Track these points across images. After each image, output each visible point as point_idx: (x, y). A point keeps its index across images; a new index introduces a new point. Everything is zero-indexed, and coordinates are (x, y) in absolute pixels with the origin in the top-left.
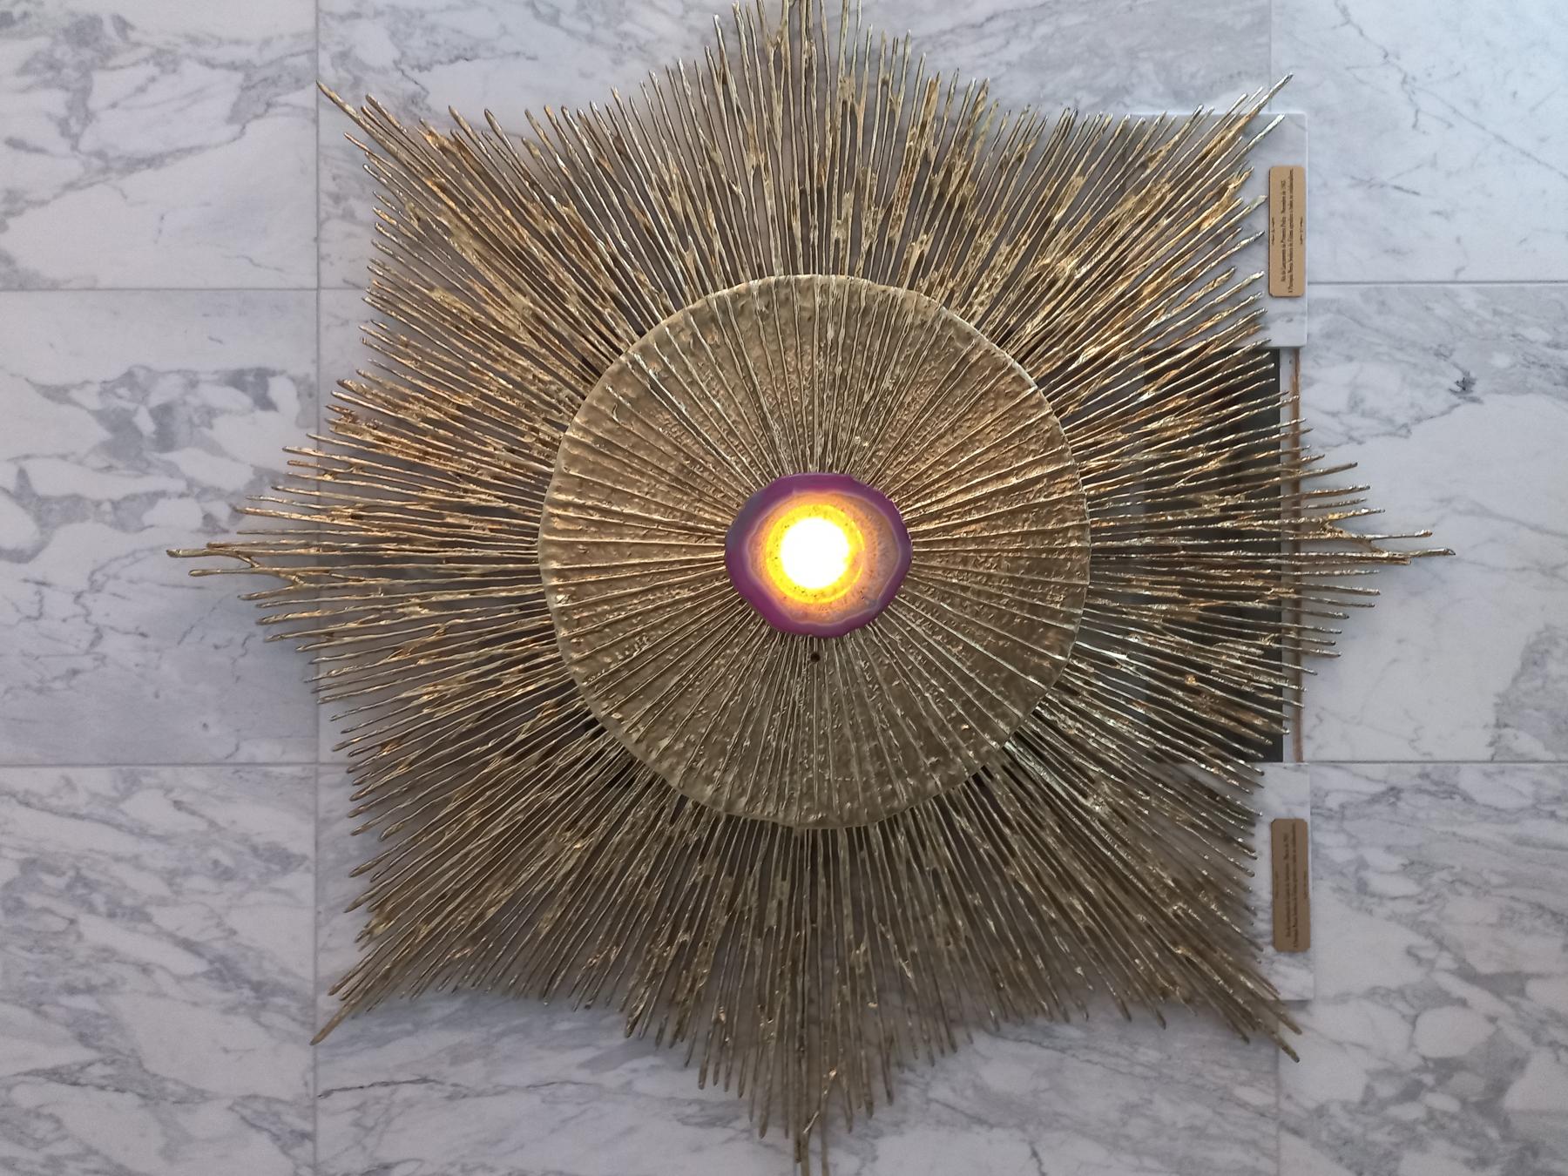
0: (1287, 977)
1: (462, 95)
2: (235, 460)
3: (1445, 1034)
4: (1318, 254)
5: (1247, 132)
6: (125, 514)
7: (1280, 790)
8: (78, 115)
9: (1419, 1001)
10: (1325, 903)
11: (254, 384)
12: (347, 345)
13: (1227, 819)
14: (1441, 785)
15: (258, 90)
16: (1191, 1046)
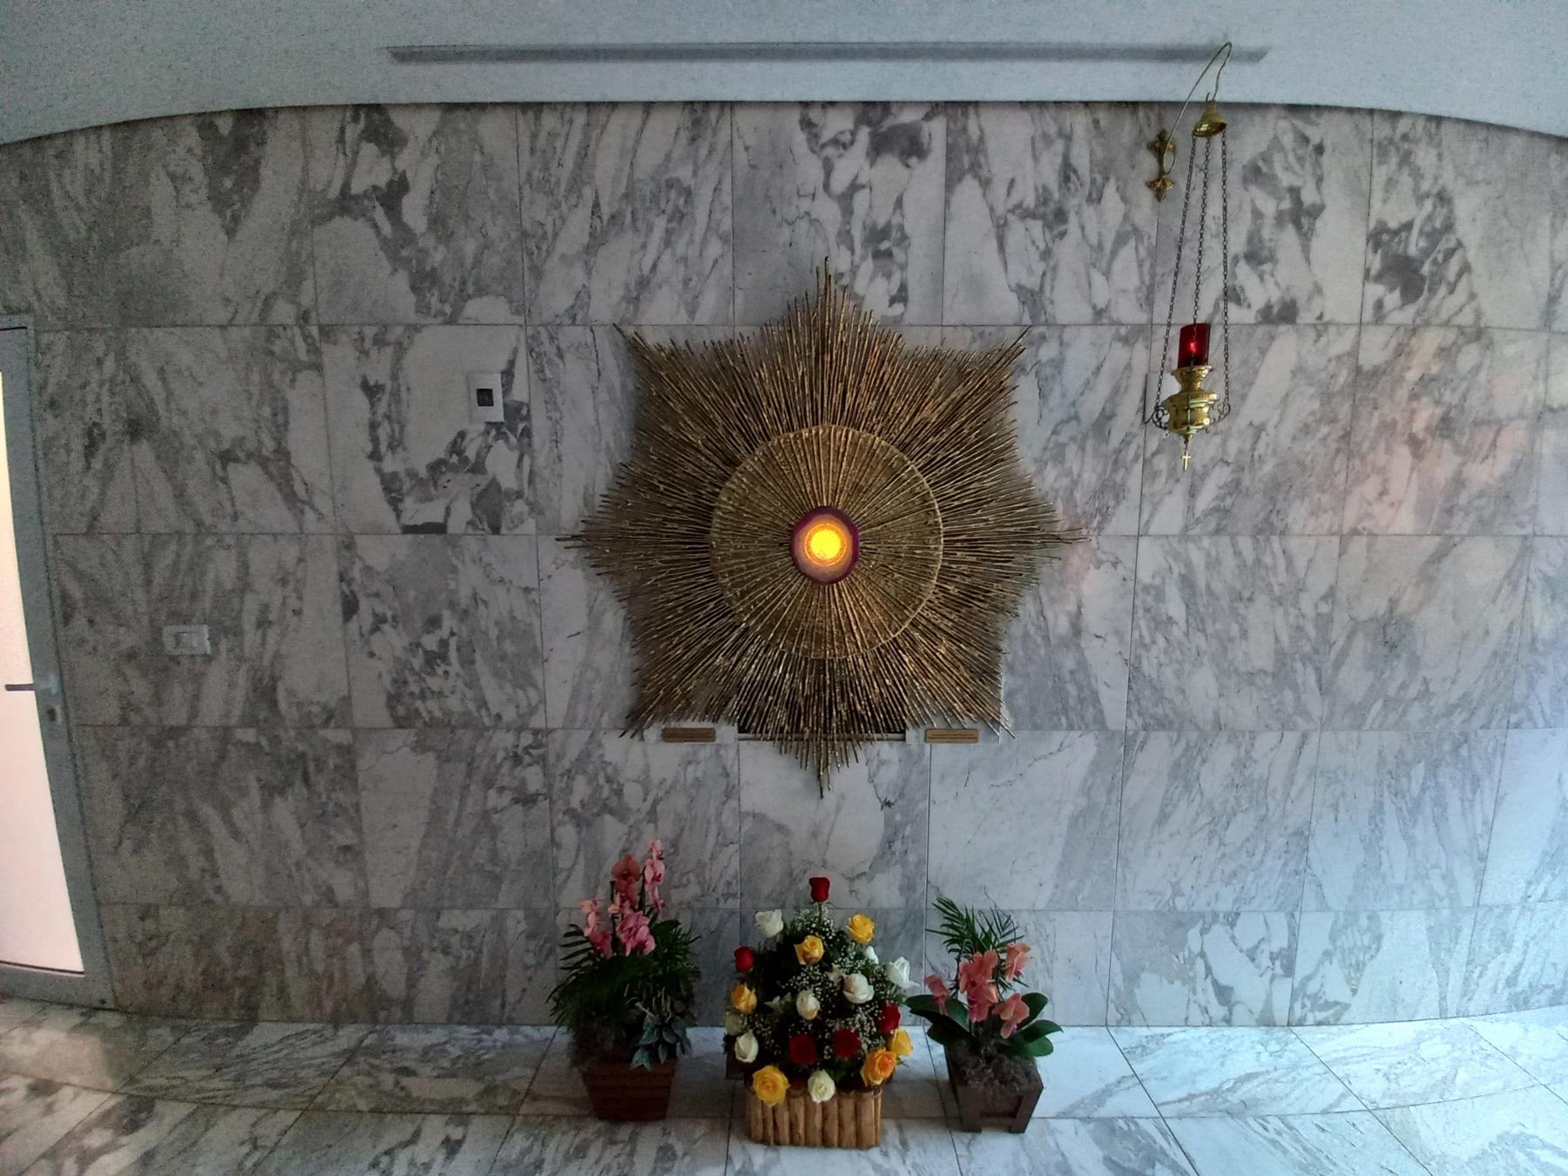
0: (652, 733)
3: (632, 793)
7: (727, 732)
10: (684, 748)
11: (901, 296)
12: (918, 340)
13: (715, 711)
14: (731, 792)
15: (1031, 298)
16: (623, 696)
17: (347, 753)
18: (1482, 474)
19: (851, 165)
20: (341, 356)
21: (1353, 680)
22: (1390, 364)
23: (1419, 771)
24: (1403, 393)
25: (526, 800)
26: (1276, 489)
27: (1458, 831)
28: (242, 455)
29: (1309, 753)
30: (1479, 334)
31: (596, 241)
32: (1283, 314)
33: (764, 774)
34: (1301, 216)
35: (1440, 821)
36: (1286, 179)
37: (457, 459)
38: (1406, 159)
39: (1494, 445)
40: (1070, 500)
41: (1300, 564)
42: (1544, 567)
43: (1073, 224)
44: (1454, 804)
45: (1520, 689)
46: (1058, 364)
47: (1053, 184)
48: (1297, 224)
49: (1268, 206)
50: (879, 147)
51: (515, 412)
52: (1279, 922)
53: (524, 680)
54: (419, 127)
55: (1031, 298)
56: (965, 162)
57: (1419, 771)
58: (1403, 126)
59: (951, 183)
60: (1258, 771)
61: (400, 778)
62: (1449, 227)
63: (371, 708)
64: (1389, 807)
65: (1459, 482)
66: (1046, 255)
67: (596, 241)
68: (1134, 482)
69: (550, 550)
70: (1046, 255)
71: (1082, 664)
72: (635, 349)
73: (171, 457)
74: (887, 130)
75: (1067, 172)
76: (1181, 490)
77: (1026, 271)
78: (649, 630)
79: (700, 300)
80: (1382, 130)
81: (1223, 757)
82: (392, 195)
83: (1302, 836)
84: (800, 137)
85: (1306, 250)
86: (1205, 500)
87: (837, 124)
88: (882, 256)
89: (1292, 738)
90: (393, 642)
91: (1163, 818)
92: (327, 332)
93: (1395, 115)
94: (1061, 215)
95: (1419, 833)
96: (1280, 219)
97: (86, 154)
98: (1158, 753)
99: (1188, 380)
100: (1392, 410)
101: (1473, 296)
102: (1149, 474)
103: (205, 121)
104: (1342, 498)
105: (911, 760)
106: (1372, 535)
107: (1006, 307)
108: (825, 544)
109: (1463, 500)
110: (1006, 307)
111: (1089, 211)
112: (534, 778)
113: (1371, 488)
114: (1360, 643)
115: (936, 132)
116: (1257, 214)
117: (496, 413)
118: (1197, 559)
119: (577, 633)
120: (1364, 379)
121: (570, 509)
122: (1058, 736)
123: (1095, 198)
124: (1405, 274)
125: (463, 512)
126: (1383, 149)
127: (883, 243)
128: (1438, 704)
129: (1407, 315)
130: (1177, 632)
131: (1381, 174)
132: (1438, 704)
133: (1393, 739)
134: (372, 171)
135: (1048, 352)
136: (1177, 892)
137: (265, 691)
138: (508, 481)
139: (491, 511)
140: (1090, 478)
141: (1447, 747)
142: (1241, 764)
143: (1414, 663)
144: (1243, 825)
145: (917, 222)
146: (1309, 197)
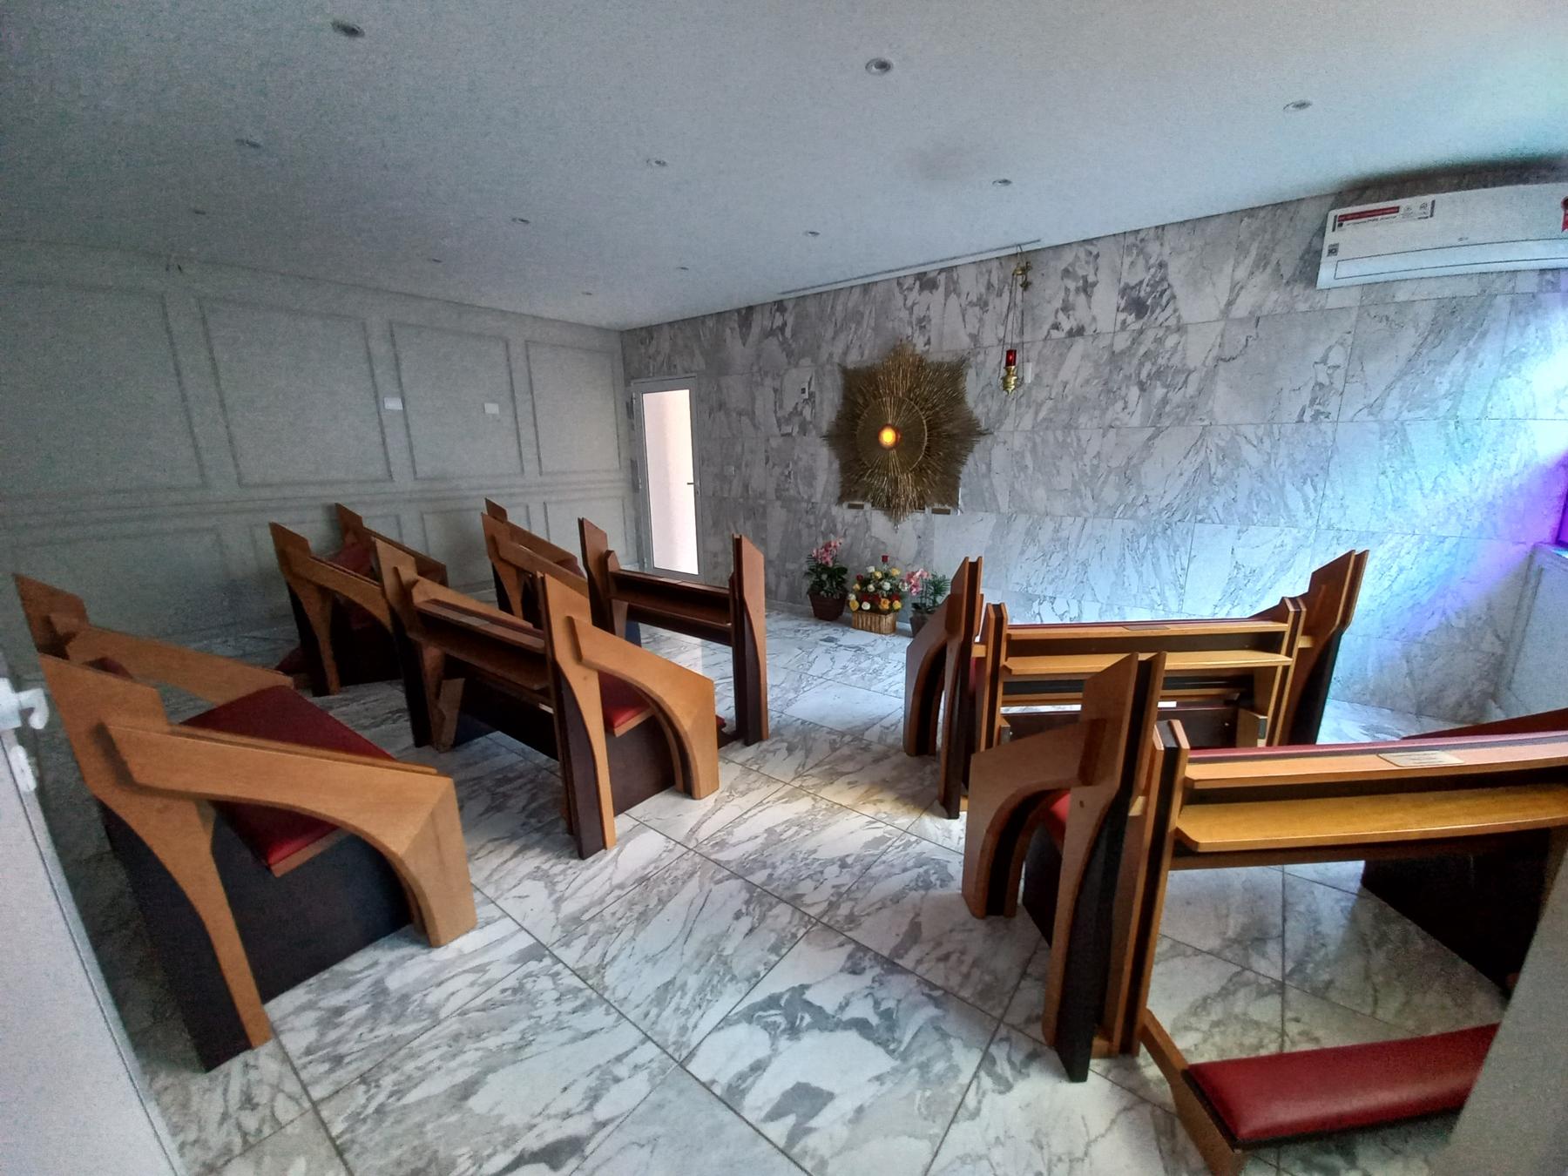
0: (845, 505)
1: (971, 374)
2: (562, 1045)
3: (839, 526)
4: (939, 517)
5: (955, 504)
6: (910, 323)
7: (868, 506)
8: (971, 304)
9: (843, 523)
10: (854, 511)
11: (928, 343)
12: (934, 357)
13: (864, 498)
14: (868, 529)
15: (975, 338)
16: (838, 492)
17: (764, 507)
18: (1176, 397)
19: (914, 296)
20: (768, 381)
21: (1110, 494)
22: (1129, 348)
23: (1143, 540)
24: (1135, 362)
25: (809, 526)
26: (1075, 410)
27: (1166, 571)
28: (792, 695)
29: (1088, 525)
30: (1181, 329)
31: (836, 333)
32: (1079, 332)
33: (879, 521)
34: (1087, 288)
35: (1156, 566)
36: (1081, 273)
37: (796, 412)
38: (1141, 252)
39: (1185, 382)
40: (988, 418)
41: (1084, 442)
42: (1216, 440)
43: (991, 307)
44: (1163, 554)
45: (1203, 502)
46: (983, 363)
47: (983, 290)
48: (1085, 291)
49: (1072, 285)
50: (922, 288)
51: (811, 395)
52: (1074, 604)
53: (811, 485)
54: (790, 306)
55: (975, 338)
56: (953, 288)
57: (1143, 540)
58: (1142, 235)
59: (947, 296)
60: (1064, 534)
61: (777, 514)
62: (1163, 279)
63: (771, 495)
64: (1128, 557)
65: (1165, 401)
66: (981, 320)
67: (836, 333)
68: (1013, 408)
69: (819, 440)
70: (981, 320)
71: (991, 484)
72: (845, 372)
73: (728, 414)
74: (926, 282)
75: (989, 286)
76: (1032, 411)
77: (972, 327)
78: (846, 469)
79: (862, 350)
80: (1131, 240)
81: (1049, 526)
82: (782, 329)
83: (1085, 564)
84: (897, 290)
85: (1089, 303)
86: (1042, 415)
87: (908, 282)
88: (922, 328)
89: (1080, 521)
90: (777, 470)
91: (1022, 552)
92: (766, 374)
93: (1137, 232)
94: (986, 304)
95: (1143, 569)
96: (1077, 290)
97: (710, 323)
98: (1021, 523)
99: (1008, 371)
100: (1129, 369)
101: (1175, 311)
102: (1019, 405)
103: (738, 311)
104: (1104, 411)
105: (927, 520)
106: (1119, 428)
107: (965, 342)
108: (888, 437)
109: (1168, 408)
110: (965, 342)
111: (997, 301)
112: (811, 519)
113: (1120, 404)
114: (1112, 477)
115: (942, 278)
116: (1067, 290)
117: (806, 396)
118: (1038, 440)
119: (823, 465)
120: (1115, 358)
121: (825, 427)
122: (981, 514)
123: (1000, 295)
124: (1138, 307)
125: (796, 429)
126: (1129, 248)
127: (923, 324)
128: (1154, 508)
129: (1137, 326)
130: (1030, 471)
131: (1127, 260)
132: (1154, 508)
133: (1131, 524)
134: (778, 322)
135: (980, 358)
136: (1029, 585)
137: (746, 487)
138: (808, 418)
139: (804, 430)
140: (995, 407)
141: (1159, 529)
142: (1056, 531)
143: (1140, 487)
144: (1056, 559)
145: (935, 314)
146: (1091, 279)
